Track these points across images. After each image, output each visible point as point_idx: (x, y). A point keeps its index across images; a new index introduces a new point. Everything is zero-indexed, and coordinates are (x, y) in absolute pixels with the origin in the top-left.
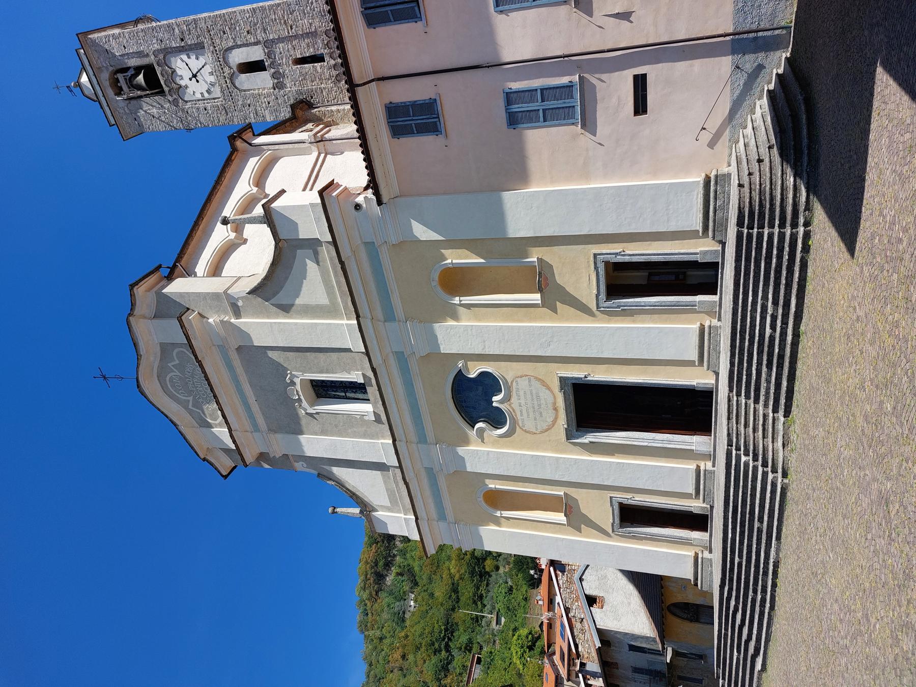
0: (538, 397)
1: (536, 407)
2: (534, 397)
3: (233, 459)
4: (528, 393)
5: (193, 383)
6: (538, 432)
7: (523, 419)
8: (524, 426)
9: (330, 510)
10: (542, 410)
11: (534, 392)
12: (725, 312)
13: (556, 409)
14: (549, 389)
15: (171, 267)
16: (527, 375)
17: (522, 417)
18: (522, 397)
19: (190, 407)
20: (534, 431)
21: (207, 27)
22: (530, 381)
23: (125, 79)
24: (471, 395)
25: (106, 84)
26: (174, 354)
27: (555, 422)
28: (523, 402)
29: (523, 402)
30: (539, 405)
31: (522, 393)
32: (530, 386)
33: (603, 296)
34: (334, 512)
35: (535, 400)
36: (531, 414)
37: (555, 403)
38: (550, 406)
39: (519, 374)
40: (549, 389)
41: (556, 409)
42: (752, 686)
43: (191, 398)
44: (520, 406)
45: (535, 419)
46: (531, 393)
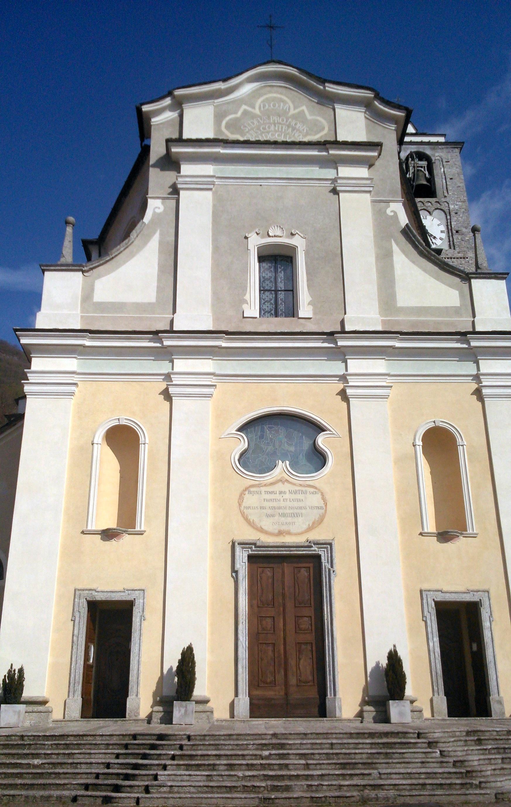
0: (296, 515)
1: (281, 511)
2: (296, 511)
3: (161, 126)
4: (301, 504)
5: (280, 123)
6: (242, 508)
7: (261, 493)
8: (250, 492)
9: (71, 219)
10: (277, 518)
11: (303, 511)
12: (194, 778)
13: (280, 533)
14: (310, 529)
15: (338, 140)
16: (326, 506)
17: (263, 493)
18: (293, 496)
19: (244, 107)
20: (244, 504)
21: (467, 258)
22: (318, 508)
23: (422, 167)
24: (281, 436)
25: (421, 149)
26: (320, 119)
27: (261, 530)
28: (287, 496)
29: (287, 496)
30: (284, 515)
31: (300, 496)
32: (312, 508)
33: (440, 597)
34: (67, 223)
35: (291, 511)
36: (267, 504)
37: (289, 533)
38: (284, 528)
39: (327, 497)
40: (310, 529)
41: (280, 533)
42: (1, 768)
43: (257, 111)
44: (281, 493)
45: (262, 508)
46: (301, 508)
